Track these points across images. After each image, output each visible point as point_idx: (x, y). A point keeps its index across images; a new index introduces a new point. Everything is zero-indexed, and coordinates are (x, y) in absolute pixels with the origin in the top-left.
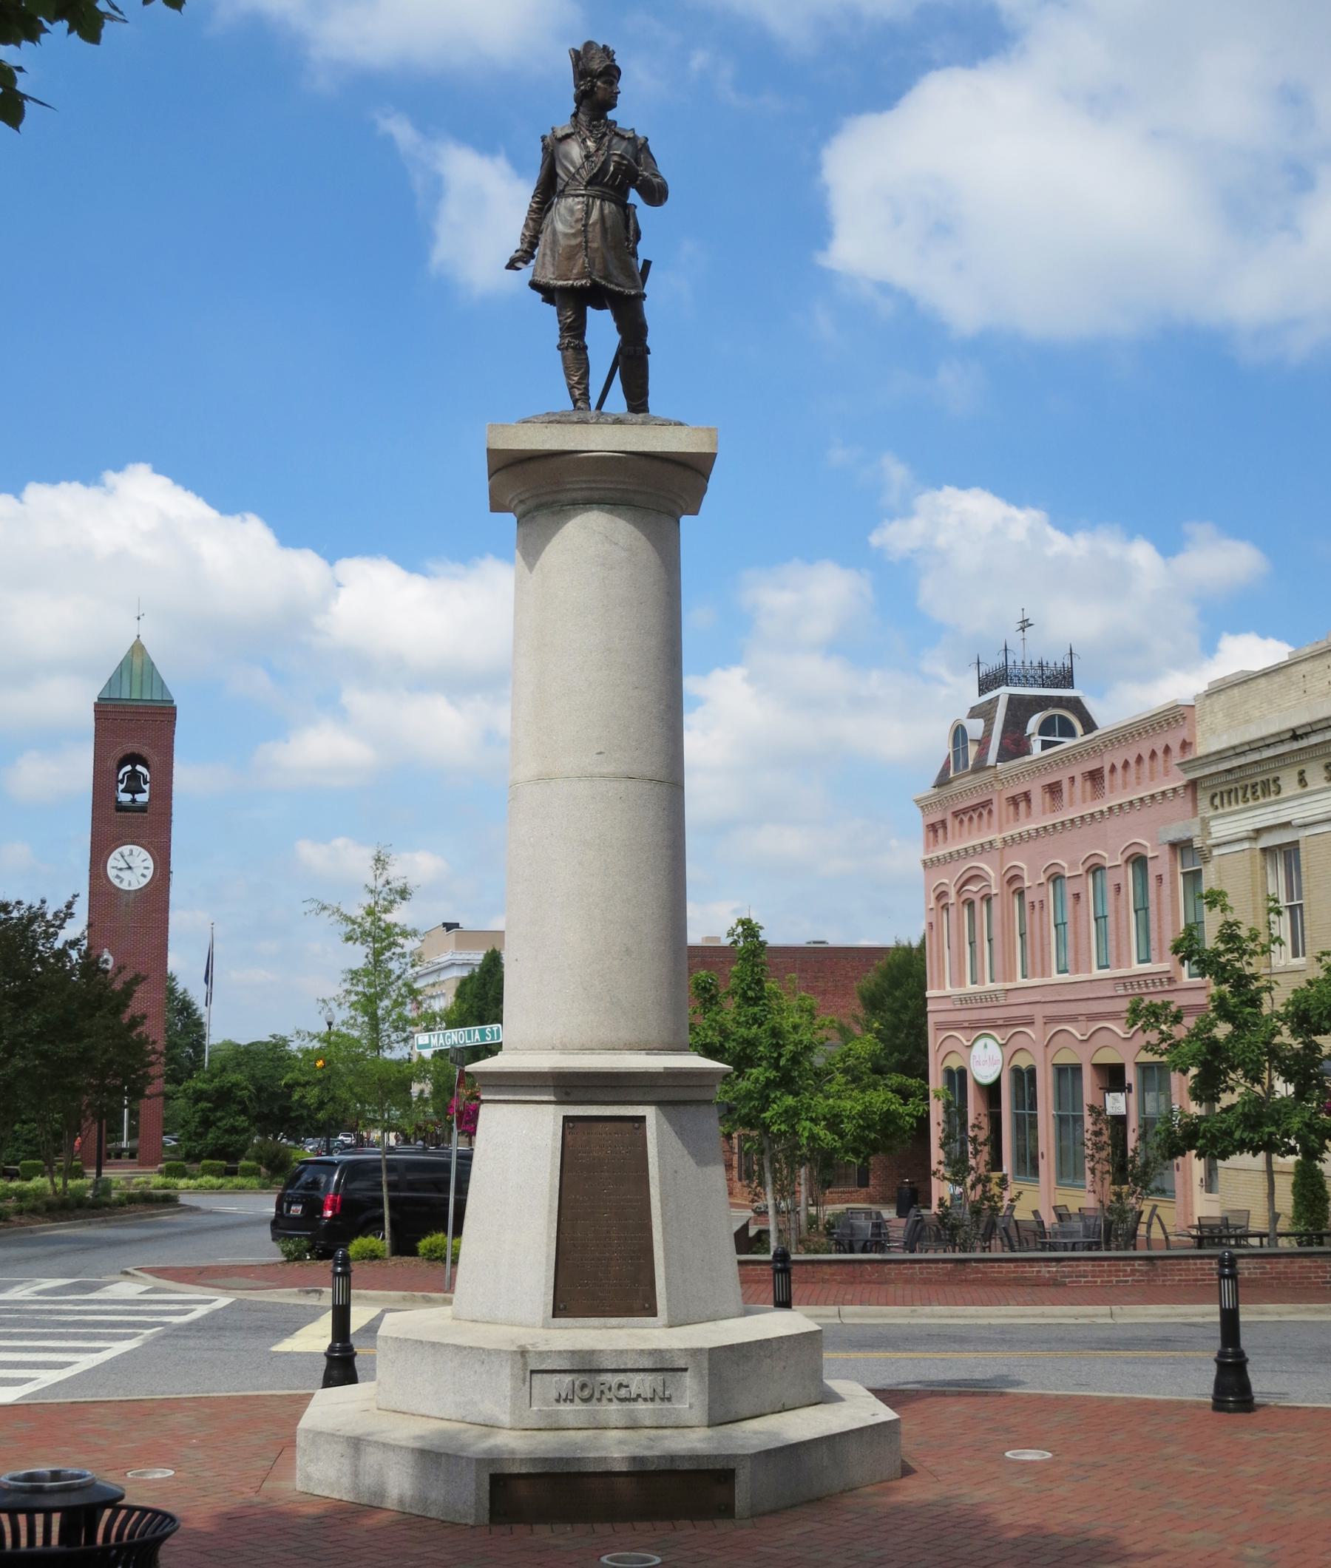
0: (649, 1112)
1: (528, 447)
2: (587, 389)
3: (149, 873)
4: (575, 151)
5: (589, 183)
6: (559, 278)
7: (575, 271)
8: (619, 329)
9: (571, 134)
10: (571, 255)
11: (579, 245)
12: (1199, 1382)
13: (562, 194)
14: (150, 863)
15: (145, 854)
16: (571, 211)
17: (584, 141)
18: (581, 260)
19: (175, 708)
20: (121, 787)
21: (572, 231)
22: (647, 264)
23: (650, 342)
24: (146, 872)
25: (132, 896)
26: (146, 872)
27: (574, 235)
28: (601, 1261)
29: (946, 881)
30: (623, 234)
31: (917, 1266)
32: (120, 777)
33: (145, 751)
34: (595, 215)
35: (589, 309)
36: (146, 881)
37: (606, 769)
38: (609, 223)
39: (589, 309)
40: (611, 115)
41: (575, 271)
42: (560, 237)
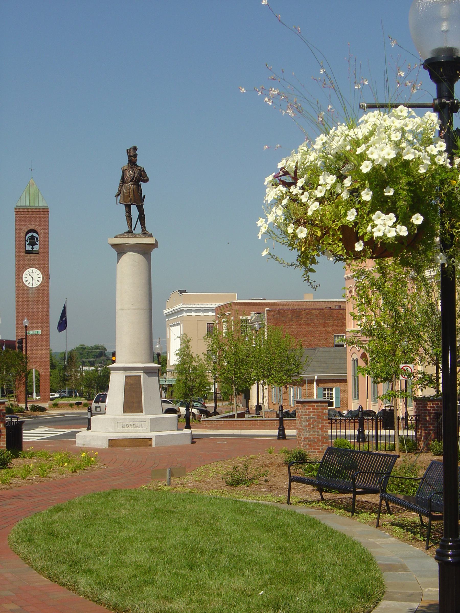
0: (142, 375)
2: (131, 225)
3: (41, 280)
5: (130, 181)
12: (276, 432)
14: (41, 276)
15: (38, 272)
19: (48, 209)
20: (27, 243)
22: (144, 196)
24: (39, 279)
25: (34, 290)
26: (39, 279)
28: (132, 403)
29: (351, 286)
30: (139, 190)
31: (276, 422)
32: (27, 239)
33: (37, 228)
34: (132, 188)
36: (39, 283)
37: (134, 307)
38: (134, 190)
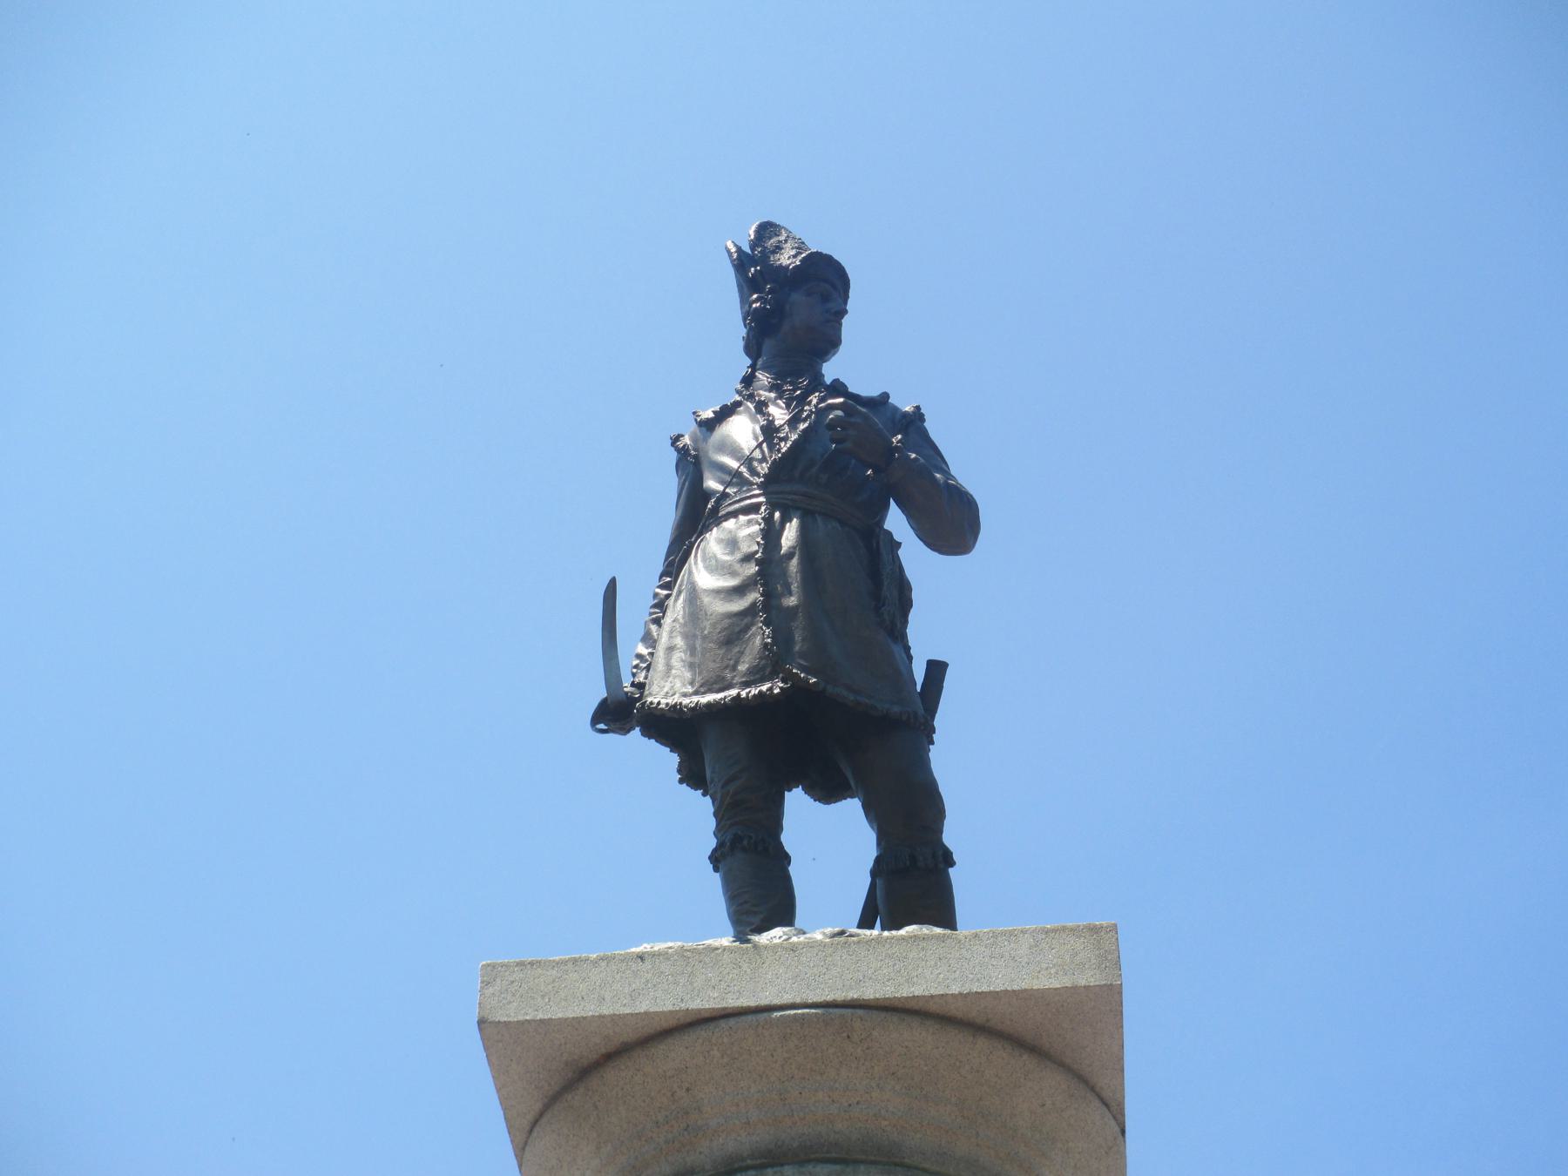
1: (590, 1009)
4: (742, 430)
6: (708, 687)
7: (742, 667)
8: (879, 844)
9: (738, 404)
10: (733, 633)
11: (751, 611)
13: (716, 519)
16: (732, 543)
17: (761, 407)
18: (760, 636)
21: (732, 582)
22: (936, 670)
23: (952, 836)
27: (739, 591)
35: (797, 802)
39: (797, 802)
40: (831, 370)
41: (742, 667)
42: (706, 600)
